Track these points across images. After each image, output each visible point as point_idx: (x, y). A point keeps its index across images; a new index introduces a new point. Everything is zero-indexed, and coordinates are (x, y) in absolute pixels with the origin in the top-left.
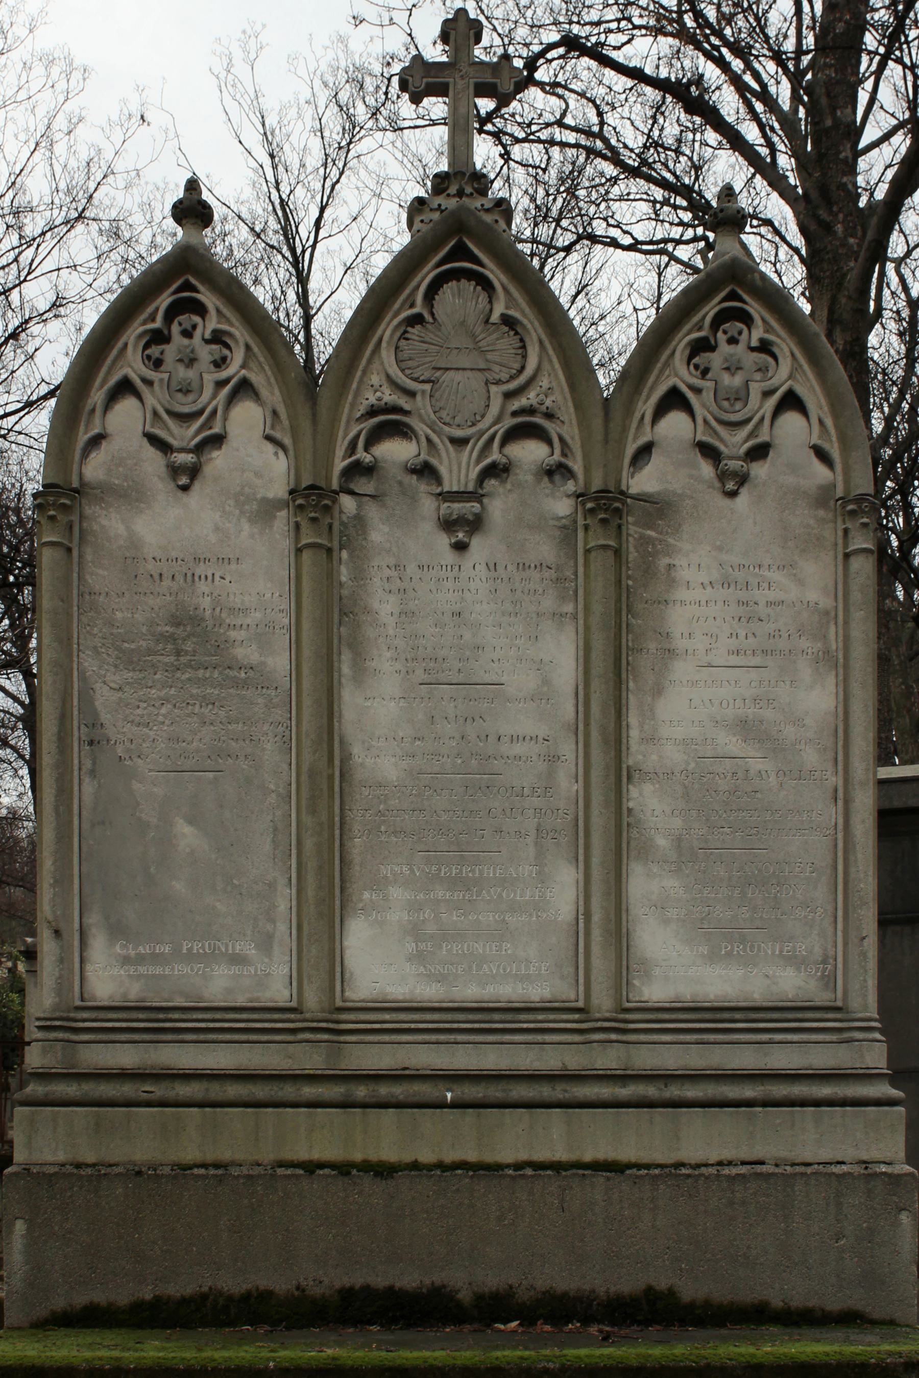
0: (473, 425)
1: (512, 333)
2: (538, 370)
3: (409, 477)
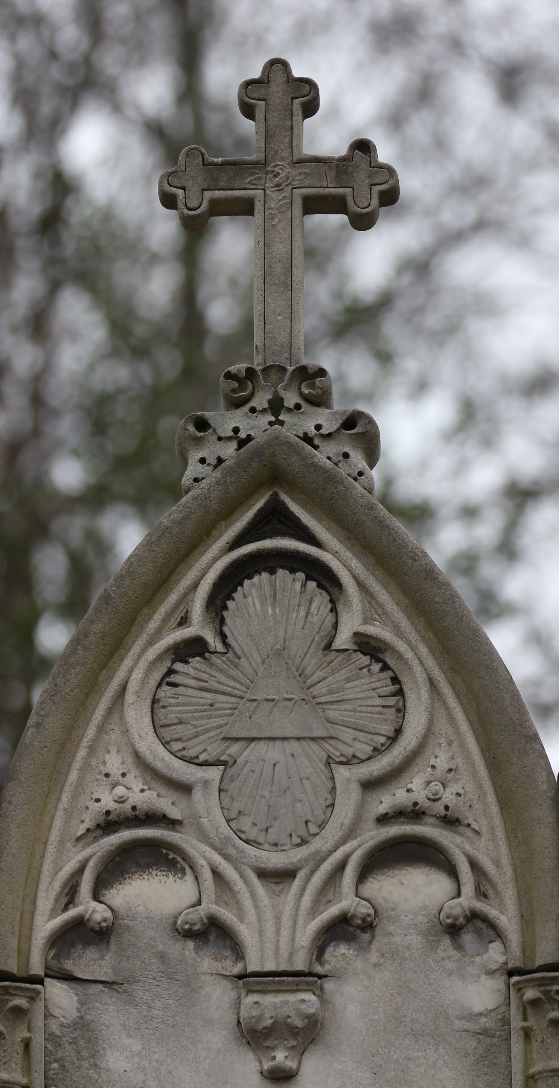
0: (304, 842)
1: (376, 667)
2: (428, 734)
3: (179, 945)
